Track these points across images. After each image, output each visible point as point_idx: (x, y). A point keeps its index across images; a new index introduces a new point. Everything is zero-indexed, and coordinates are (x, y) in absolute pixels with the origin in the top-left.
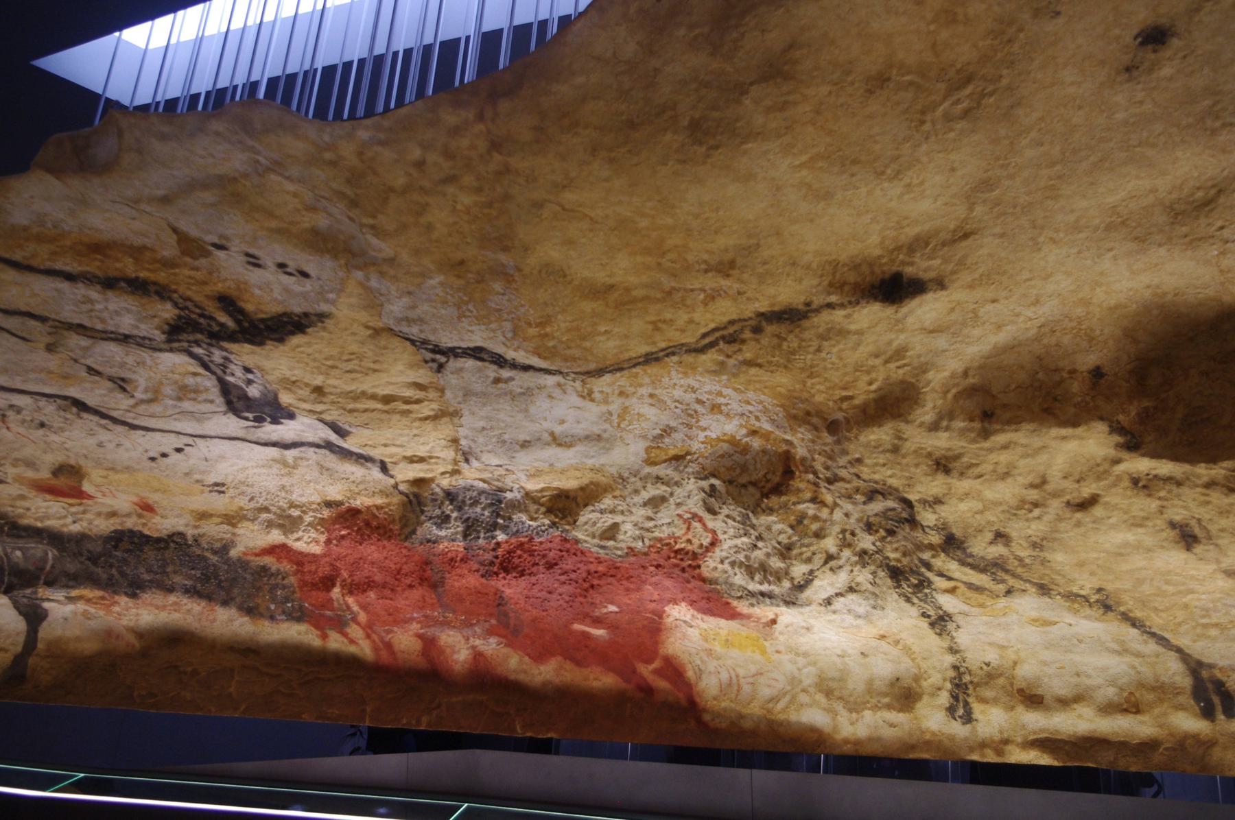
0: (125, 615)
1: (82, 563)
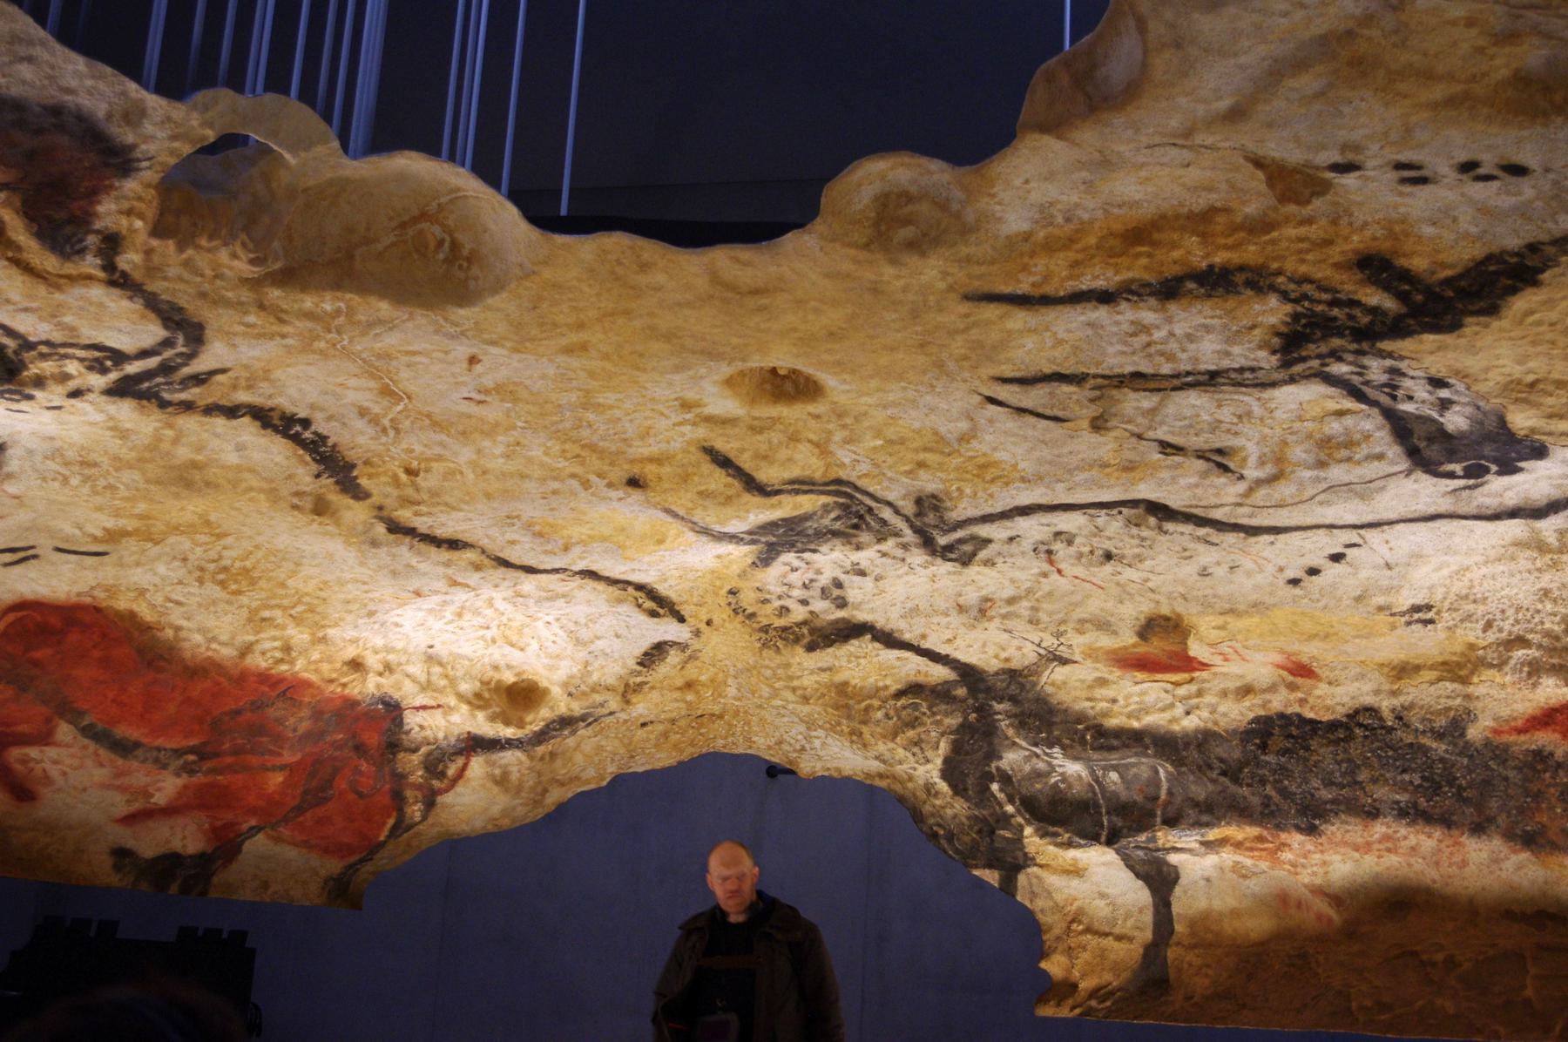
0: (1303, 866)
1: (1213, 781)
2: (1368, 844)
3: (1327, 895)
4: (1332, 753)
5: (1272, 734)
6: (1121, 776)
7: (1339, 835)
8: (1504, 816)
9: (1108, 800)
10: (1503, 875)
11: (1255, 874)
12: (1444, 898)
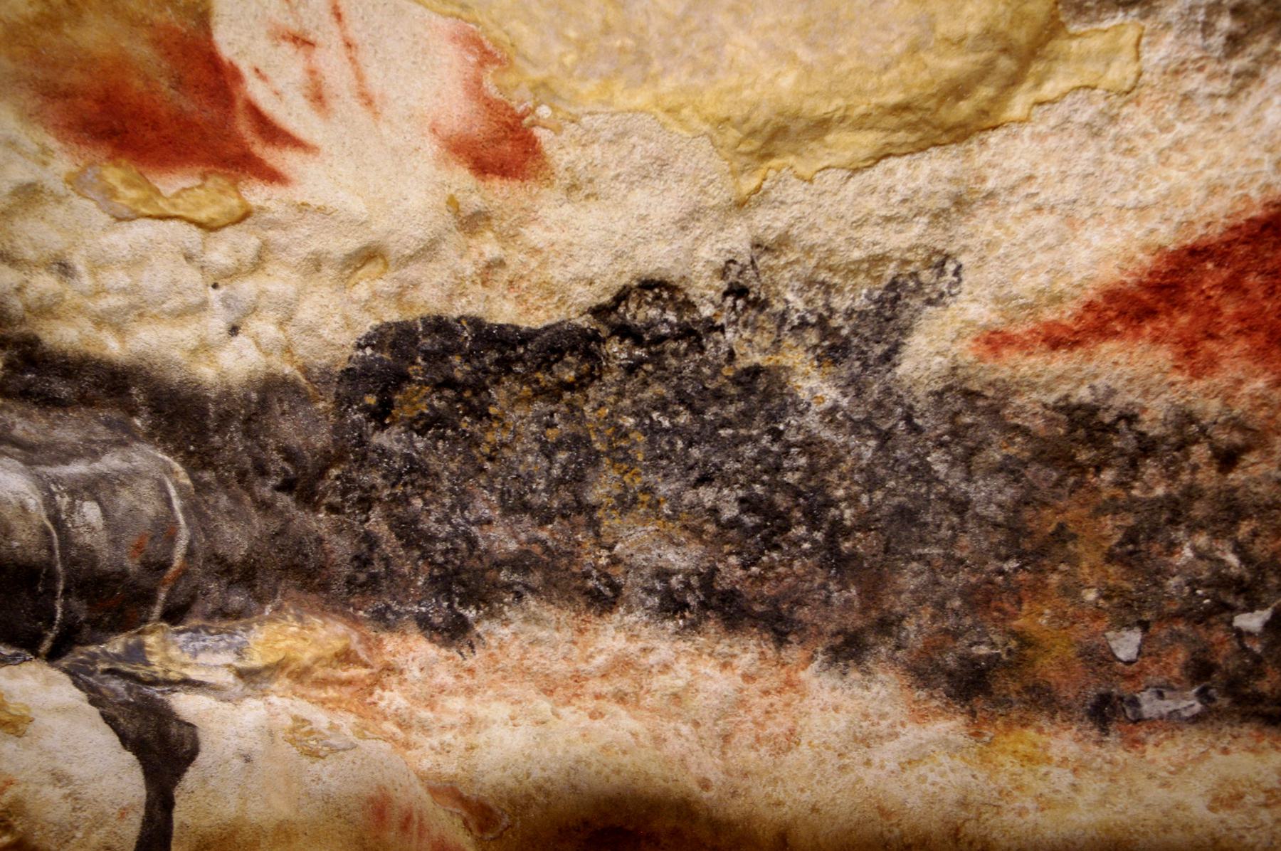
0: (425, 728)
1: (265, 506)
2: (578, 678)
3: (463, 801)
4: (538, 418)
5: (407, 378)
6: (105, 513)
7: (514, 650)
8: (927, 612)
9: (71, 563)
10: (869, 776)
11: (334, 750)
12: (719, 826)
